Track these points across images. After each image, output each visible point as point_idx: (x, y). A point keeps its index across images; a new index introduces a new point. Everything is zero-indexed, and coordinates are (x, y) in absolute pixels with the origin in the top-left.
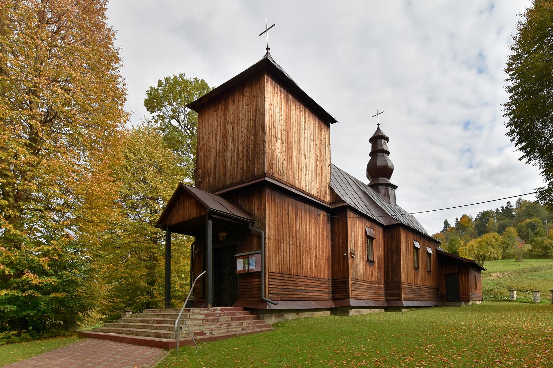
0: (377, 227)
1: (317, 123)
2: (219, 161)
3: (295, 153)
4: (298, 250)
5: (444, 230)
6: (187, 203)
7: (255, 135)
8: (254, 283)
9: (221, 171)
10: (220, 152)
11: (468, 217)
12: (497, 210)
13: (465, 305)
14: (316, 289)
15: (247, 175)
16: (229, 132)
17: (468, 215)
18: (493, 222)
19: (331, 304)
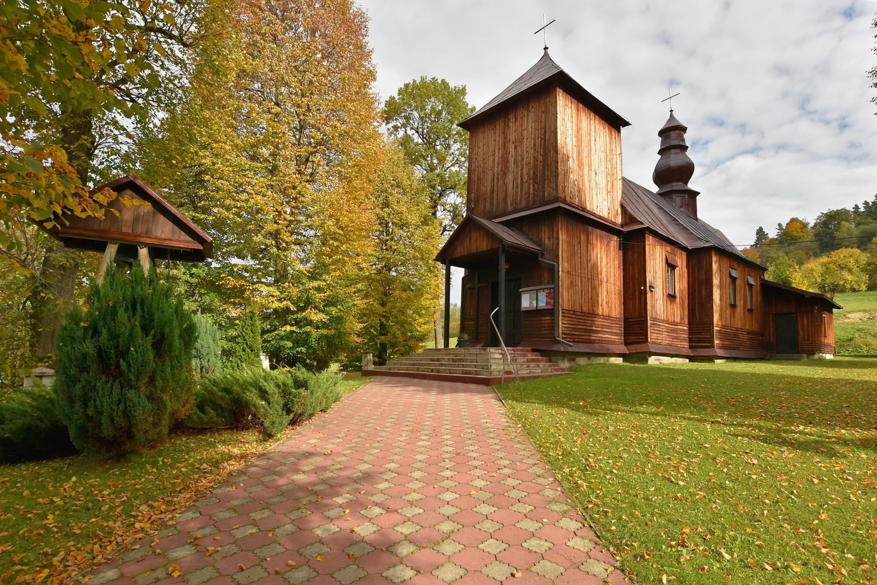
0: (678, 252)
1: (607, 130)
3: (586, 171)
4: (590, 284)
5: (756, 245)
6: (474, 235)
7: (545, 155)
9: (500, 195)
10: (498, 174)
11: (801, 222)
12: (857, 207)
13: (808, 358)
14: (607, 330)
15: (534, 201)
17: (800, 219)
18: (849, 229)
19: (623, 349)
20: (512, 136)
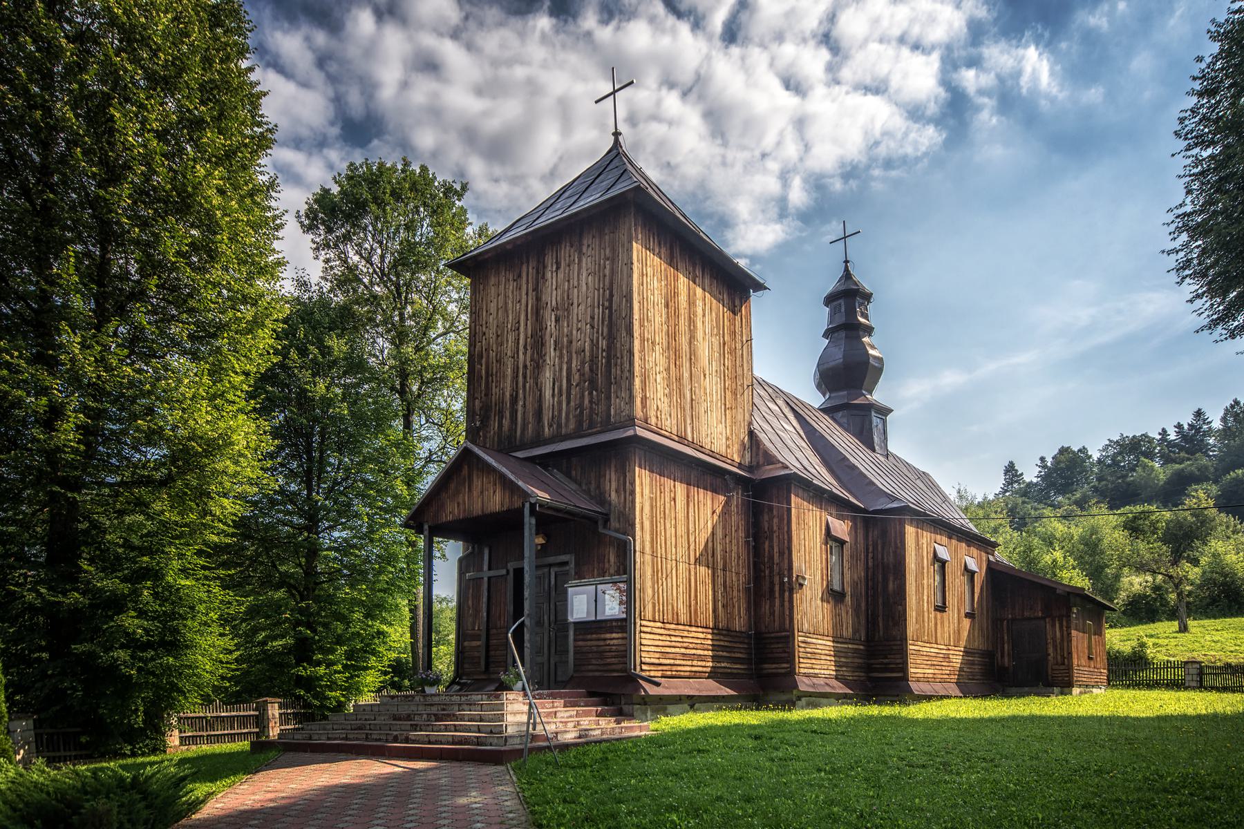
2: (524, 386)
7: (611, 338)
8: (608, 642)
10: (525, 367)
16: (549, 327)
20: (551, 296)
